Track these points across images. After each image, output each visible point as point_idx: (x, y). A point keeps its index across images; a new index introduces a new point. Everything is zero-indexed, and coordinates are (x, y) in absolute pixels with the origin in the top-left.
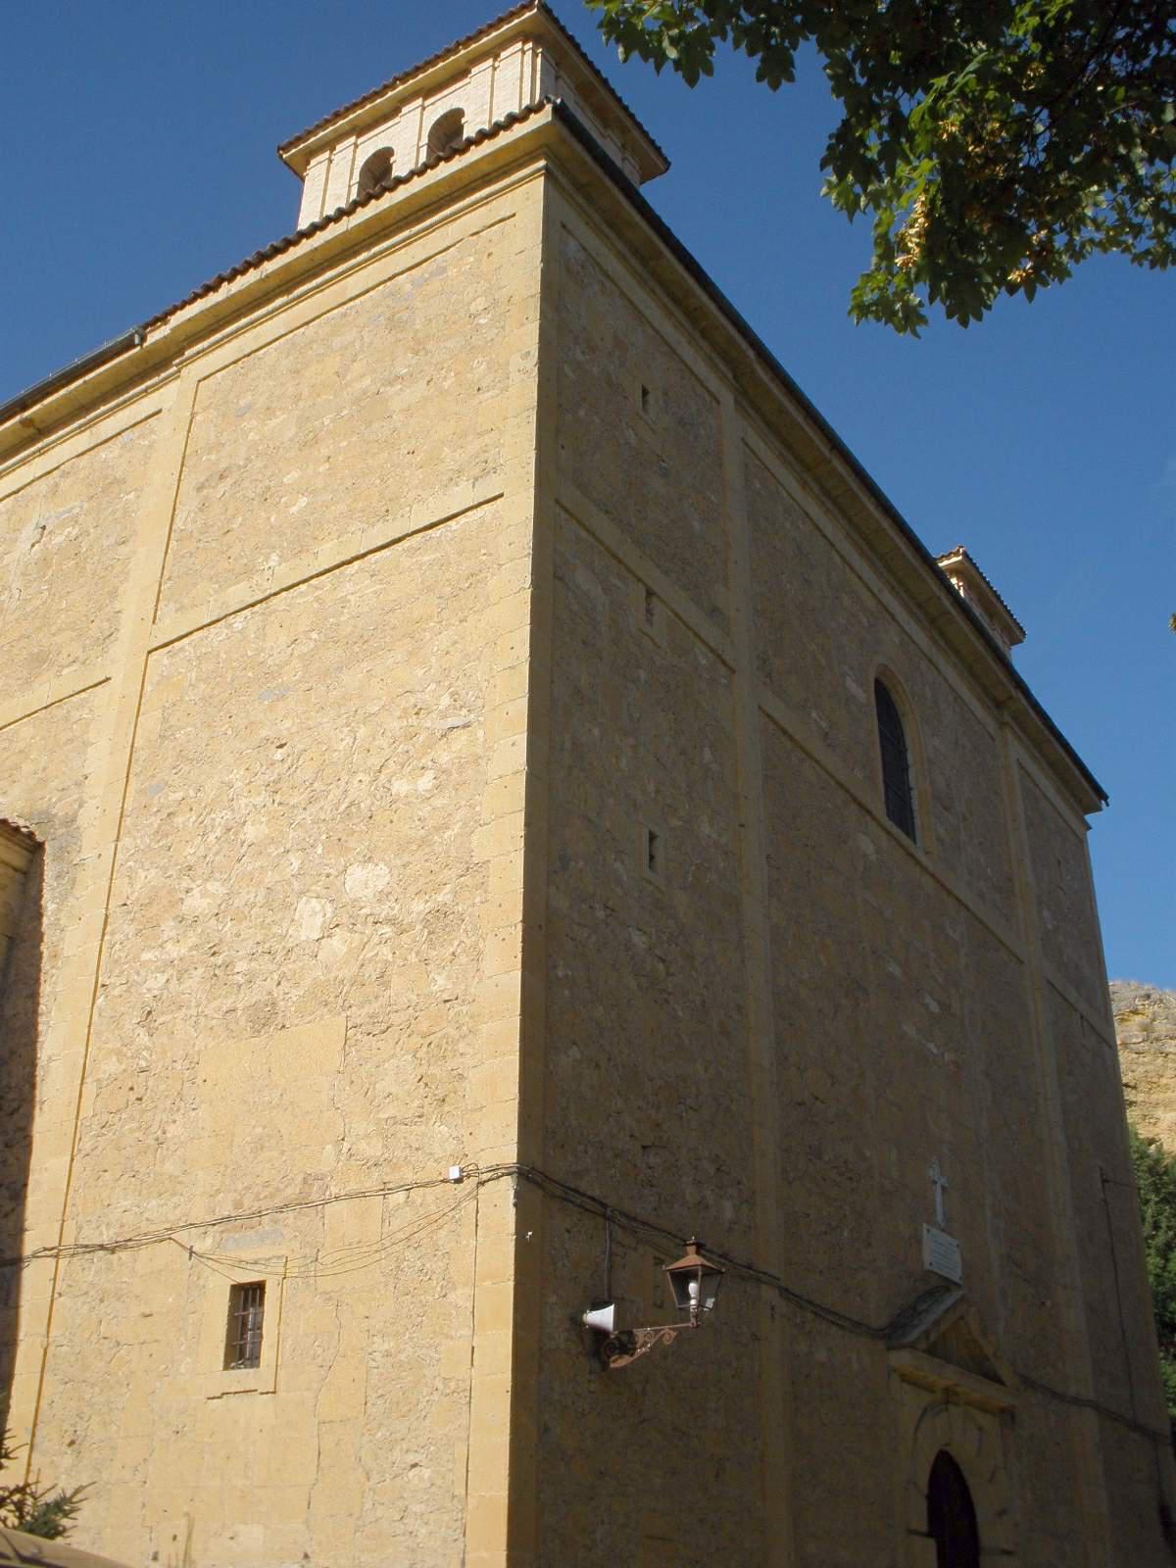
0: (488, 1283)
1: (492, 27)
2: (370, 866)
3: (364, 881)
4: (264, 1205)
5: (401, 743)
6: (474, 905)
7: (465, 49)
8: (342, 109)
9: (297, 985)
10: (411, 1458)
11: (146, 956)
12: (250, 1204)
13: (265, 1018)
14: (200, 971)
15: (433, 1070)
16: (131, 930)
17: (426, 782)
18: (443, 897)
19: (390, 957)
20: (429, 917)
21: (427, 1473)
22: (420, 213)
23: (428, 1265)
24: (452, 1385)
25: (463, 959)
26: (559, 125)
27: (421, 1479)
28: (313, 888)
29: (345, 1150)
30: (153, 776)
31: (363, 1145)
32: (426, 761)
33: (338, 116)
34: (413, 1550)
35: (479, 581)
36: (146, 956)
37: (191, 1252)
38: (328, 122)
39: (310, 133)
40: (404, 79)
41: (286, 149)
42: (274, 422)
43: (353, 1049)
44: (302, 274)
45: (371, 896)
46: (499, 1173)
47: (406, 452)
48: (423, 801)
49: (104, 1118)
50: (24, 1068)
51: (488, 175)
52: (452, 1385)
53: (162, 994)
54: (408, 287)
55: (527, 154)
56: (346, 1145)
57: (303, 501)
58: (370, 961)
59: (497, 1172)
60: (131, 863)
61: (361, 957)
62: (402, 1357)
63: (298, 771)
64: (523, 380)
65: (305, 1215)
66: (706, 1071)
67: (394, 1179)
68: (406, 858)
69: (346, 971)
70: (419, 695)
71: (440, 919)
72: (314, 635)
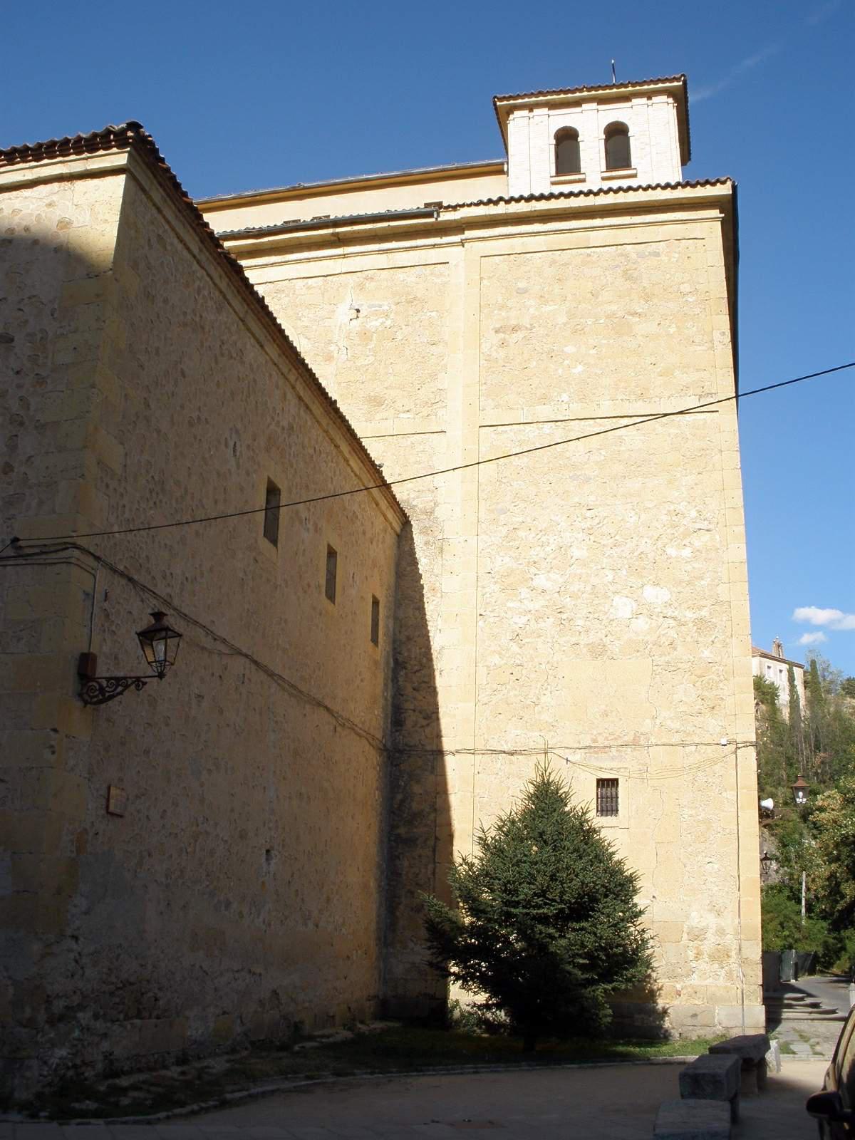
0: (745, 791)
1: (652, 82)
2: (658, 588)
3: (655, 595)
4: (612, 743)
5: (668, 528)
6: (722, 621)
7: (633, 87)
8: (545, 91)
9: (619, 639)
10: (708, 860)
11: (510, 604)
12: (601, 741)
13: (598, 651)
14: (552, 620)
15: (706, 694)
16: (496, 588)
17: (687, 553)
18: (704, 613)
19: (676, 636)
20: (696, 621)
21: (716, 866)
22: (637, 210)
23: (710, 780)
24: (727, 831)
25: (718, 645)
26: (730, 197)
27: (713, 868)
28: (623, 591)
29: (658, 723)
30: (498, 503)
31: (669, 722)
32: (686, 542)
33: (541, 93)
34: (711, 896)
35: (706, 455)
36: (510, 604)
37: (567, 760)
38: (532, 95)
39: (518, 97)
40: (589, 90)
41: (501, 99)
42: (549, 308)
43: (658, 676)
44: (554, 215)
45: (660, 603)
46: (748, 744)
47: (650, 363)
48: (686, 563)
49: (495, 686)
50: (420, 648)
51: (683, 204)
52: (727, 831)
53: (525, 628)
54: (634, 256)
55: (709, 202)
56: (658, 721)
57: (580, 368)
58: (663, 635)
59: (747, 744)
60: (489, 550)
61: (658, 632)
62: (700, 818)
63: (604, 527)
64: (723, 348)
65: (638, 750)
66: (516, 690)
67: (688, 740)
68: (680, 589)
69: (649, 637)
70: (676, 505)
71: (702, 625)
72: (603, 452)
